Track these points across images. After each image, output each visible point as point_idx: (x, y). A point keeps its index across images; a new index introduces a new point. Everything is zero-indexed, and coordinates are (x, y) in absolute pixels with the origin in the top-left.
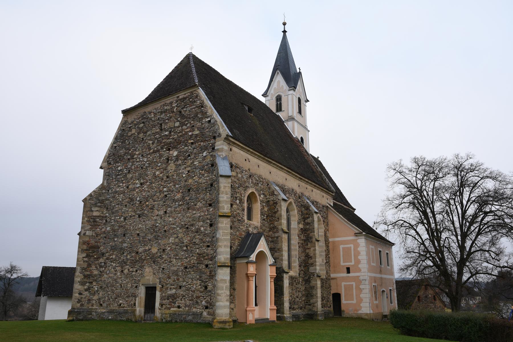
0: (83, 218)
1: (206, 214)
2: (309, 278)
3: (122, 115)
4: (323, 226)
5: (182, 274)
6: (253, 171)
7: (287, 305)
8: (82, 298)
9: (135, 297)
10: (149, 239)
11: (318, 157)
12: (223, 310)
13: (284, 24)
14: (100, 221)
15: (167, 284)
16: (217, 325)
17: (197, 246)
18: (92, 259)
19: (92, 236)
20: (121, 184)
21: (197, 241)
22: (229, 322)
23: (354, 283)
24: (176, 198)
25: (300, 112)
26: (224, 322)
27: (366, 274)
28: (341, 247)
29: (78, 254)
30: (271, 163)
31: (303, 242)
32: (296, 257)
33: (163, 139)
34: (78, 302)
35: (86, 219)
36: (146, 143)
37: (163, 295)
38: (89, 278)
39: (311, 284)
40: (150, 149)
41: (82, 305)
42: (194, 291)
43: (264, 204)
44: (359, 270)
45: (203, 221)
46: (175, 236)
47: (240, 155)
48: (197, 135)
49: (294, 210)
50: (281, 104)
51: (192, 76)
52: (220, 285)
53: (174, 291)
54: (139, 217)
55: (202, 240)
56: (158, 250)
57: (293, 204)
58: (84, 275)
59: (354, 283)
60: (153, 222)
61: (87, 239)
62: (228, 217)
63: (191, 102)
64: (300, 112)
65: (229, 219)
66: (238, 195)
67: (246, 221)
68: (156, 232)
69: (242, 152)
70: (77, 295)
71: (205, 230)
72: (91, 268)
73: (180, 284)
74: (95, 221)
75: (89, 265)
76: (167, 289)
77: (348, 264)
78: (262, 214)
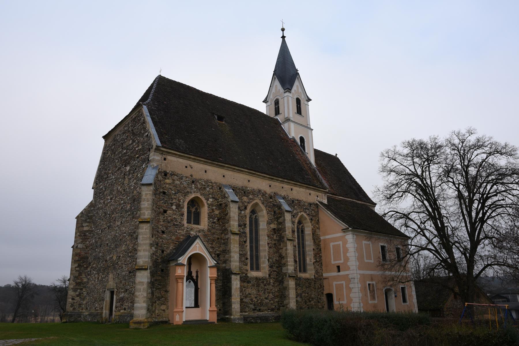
0: (76, 234)
2: (283, 278)
4: (310, 224)
6: (196, 176)
7: (236, 306)
8: (74, 303)
11: (336, 155)
12: (140, 311)
13: (283, 30)
16: (132, 326)
22: (144, 322)
23: (344, 282)
25: (299, 111)
26: (139, 323)
27: (355, 272)
28: (332, 244)
29: (72, 265)
30: (224, 166)
31: (276, 242)
32: (265, 258)
35: (78, 234)
39: (284, 285)
41: (74, 309)
43: (214, 208)
44: (348, 269)
46: (125, 243)
47: (177, 163)
49: (262, 210)
50: (278, 107)
52: (138, 287)
57: (261, 204)
59: (344, 282)
61: (79, 251)
62: (148, 222)
64: (299, 111)
65: (149, 225)
66: (174, 201)
67: (186, 225)
69: (181, 160)
70: (70, 300)
72: (82, 277)
74: (85, 235)
75: (80, 274)
77: (338, 262)
78: (210, 216)
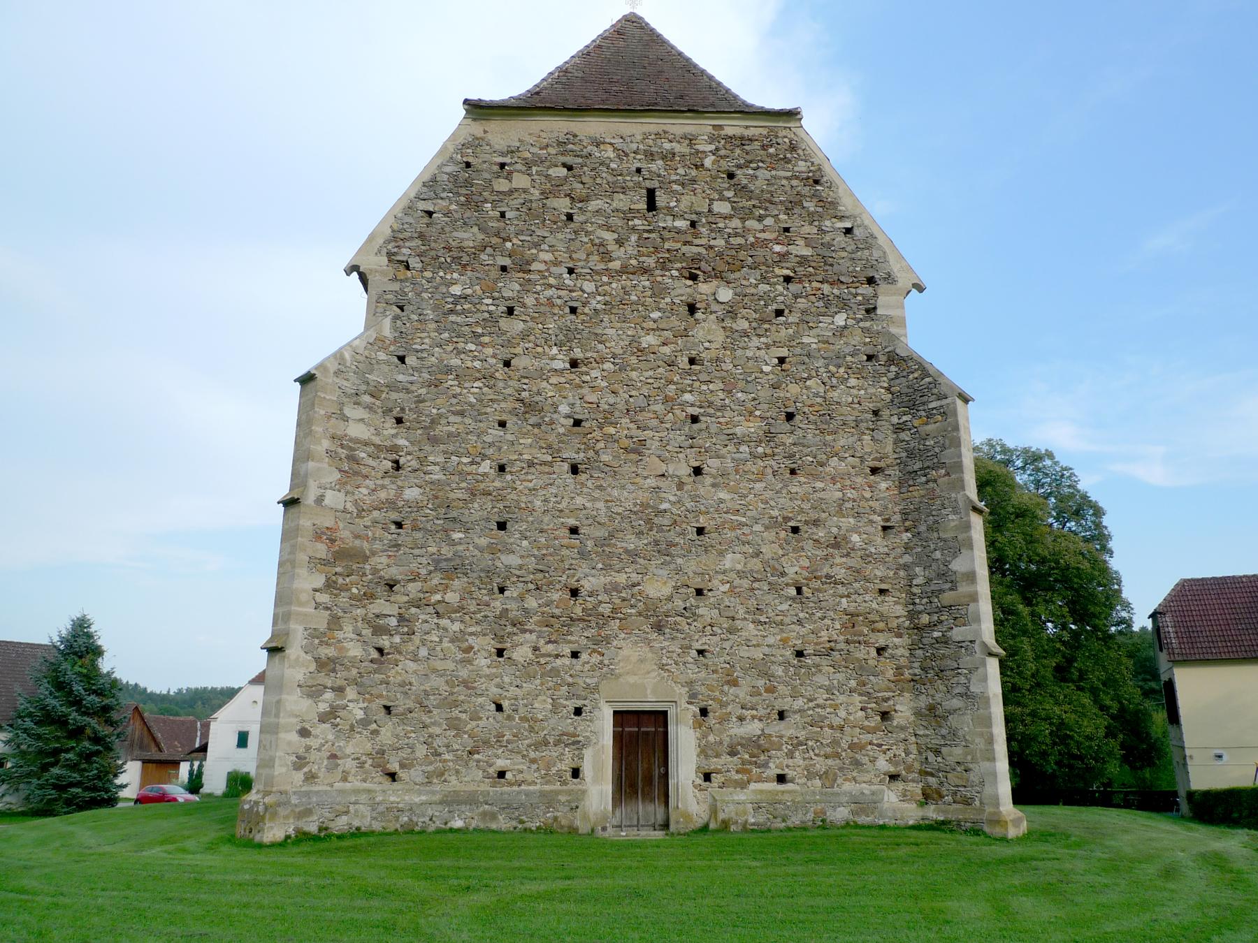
1: (868, 495)
5: (786, 671)
8: (308, 748)
9: (578, 745)
10: (627, 551)
14: (371, 462)
15: (723, 705)
17: (841, 590)
18: (343, 599)
19: (345, 511)
20: (471, 347)
21: (840, 573)
34: (297, 767)
36: (587, 233)
37: (711, 738)
40: (606, 256)
41: (311, 777)
42: (841, 728)
48: (803, 261)
51: (632, 75)
54: (575, 470)
56: (676, 588)
58: (317, 660)
60: (642, 496)
63: (770, 155)
68: (660, 530)
70: (294, 737)
71: (868, 543)
72: (340, 635)
73: (780, 705)
74: (352, 459)
75: (335, 623)
76: (724, 720)
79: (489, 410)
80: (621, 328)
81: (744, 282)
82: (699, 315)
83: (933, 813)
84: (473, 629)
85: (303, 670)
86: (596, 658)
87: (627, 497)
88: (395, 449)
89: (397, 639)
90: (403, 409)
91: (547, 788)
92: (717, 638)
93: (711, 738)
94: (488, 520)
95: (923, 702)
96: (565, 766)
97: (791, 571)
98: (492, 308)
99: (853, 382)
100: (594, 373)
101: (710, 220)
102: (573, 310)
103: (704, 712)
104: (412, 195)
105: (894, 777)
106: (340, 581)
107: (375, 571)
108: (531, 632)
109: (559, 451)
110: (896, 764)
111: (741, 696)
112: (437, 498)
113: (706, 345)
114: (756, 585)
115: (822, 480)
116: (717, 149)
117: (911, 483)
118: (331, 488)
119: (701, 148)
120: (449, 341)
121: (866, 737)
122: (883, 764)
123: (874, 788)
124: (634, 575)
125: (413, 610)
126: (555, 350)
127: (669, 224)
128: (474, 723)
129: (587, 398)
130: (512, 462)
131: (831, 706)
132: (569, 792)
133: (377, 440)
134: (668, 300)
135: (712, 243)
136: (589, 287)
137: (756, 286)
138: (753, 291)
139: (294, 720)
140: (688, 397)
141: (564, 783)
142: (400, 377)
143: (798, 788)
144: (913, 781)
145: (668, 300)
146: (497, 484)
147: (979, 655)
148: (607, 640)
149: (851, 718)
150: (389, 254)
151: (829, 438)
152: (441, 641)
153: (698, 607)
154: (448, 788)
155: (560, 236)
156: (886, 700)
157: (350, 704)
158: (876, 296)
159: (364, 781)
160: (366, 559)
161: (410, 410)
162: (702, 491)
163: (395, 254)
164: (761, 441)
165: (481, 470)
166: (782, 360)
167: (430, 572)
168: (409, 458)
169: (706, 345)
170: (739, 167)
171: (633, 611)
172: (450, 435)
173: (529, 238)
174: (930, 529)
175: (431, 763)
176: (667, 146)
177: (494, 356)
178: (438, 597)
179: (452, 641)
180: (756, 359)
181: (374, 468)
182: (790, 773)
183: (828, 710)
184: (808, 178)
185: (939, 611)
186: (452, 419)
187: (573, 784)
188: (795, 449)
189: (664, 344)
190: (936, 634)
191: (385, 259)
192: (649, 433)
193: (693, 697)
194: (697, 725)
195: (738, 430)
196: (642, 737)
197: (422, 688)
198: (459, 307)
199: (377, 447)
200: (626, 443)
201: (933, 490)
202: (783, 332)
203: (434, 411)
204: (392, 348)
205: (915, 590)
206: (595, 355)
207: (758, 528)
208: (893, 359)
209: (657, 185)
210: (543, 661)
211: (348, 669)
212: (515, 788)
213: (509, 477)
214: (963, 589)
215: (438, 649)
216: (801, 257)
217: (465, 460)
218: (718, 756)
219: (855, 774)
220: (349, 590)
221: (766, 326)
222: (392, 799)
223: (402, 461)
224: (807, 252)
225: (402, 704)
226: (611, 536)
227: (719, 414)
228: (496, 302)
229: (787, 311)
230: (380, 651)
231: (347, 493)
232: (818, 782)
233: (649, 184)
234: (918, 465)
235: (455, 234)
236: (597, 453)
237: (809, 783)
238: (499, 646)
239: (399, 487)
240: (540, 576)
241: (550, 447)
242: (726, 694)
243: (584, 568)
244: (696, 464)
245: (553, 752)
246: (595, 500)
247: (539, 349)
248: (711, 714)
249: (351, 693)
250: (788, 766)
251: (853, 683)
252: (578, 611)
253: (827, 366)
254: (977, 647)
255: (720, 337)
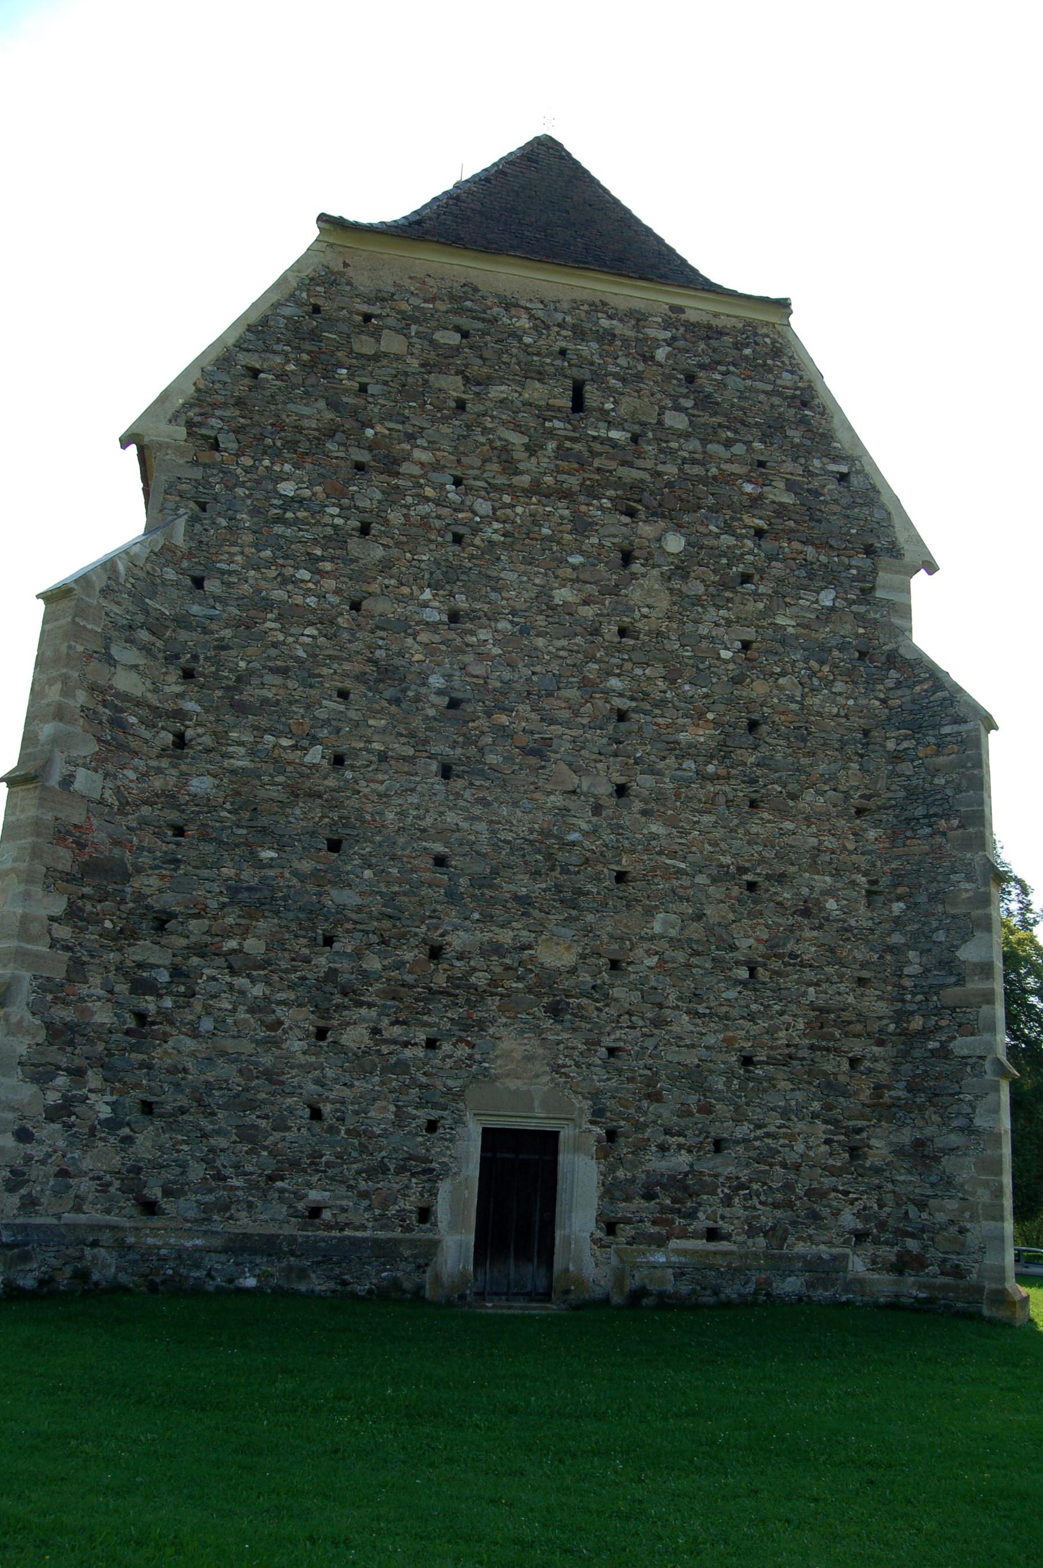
1: (850, 846)
3: (313, 232)
5: (728, 1084)
8: (28, 1159)
9: (431, 1175)
10: (516, 898)
15: (640, 1127)
17: (809, 974)
18: (91, 936)
19: (102, 802)
20: (304, 574)
21: (809, 952)
24: (682, 737)
33: (594, 454)
34: (12, 1187)
36: (485, 431)
37: (620, 1174)
38: (71, 1043)
40: (510, 467)
41: (30, 1203)
42: (797, 1167)
45: (837, 873)
48: (781, 510)
53: (684, 1159)
54: (446, 772)
55: (832, 951)
56: (583, 956)
58: (49, 1025)
68: (565, 871)
71: (847, 911)
72: (83, 990)
73: (715, 1131)
74: (118, 723)
75: (77, 970)
76: (641, 1147)
79: (325, 671)
80: (525, 573)
81: (702, 529)
82: (636, 567)
83: (911, 1287)
84: (281, 996)
85: (28, 1040)
86: (463, 1051)
87: (521, 822)
88: (180, 715)
89: (168, 1003)
90: (195, 657)
91: (381, 1234)
92: (637, 1033)
93: (620, 1174)
94: (313, 834)
95: (906, 1137)
96: (409, 1204)
97: (744, 943)
98: (339, 521)
99: (839, 687)
100: (484, 634)
101: (659, 435)
102: (458, 539)
103: (612, 1135)
104: (231, 342)
105: (860, 1237)
106: (89, 907)
107: (139, 897)
108: (370, 1005)
109: (426, 742)
110: (867, 1219)
111: (666, 1114)
112: (239, 794)
113: (645, 610)
114: (694, 960)
115: (793, 818)
116: (674, 338)
117: (909, 833)
118: (84, 766)
119: (652, 333)
120: (270, 563)
121: (828, 1182)
122: (848, 1219)
123: (835, 1251)
124: (525, 933)
125: (195, 960)
126: (427, 594)
127: (603, 433)
128: (278, 1135)
129: (470, 669)
130: (355, 753)
131: (785, 1136)
132: (413, 1243)
133: (153, 699)
134: (595, 540)
135: (660, 468)
136: (484, 507)
137: (717, 536)
138: (714, 543)
139: (10, 1116)
140: (614, 682)
141: (408, 1229)
142: (195, 609)
143: (734, 1248)
144: (886, 1243)
145: (595, 540)
146: (331, 782)
147: (989, 1076)
148: (481, 1025)
149: (812, 1154)
150: (190, 424)
151: (804, 761)
152: (234, 1010)
153: (612, 986)
154: (232, 1228)
155: (445, 429)
156: (859, 1131)
157: (92, 1096)
158: (874, 571)
159: (108, 1211)
160: (127, 877)
161: (206, 658)
162: (626, 820)
163: (200, 425)
164: (712, 757)
165: (308, 759)
166: (746, 645)
167: (224, 905)
168: (200, 730)
169: (645, 610)
170: (702, 367)
171: (520, 985)
172: (265, 701)
173: (400, 427)
174: (932, 898)
175: (211, 1191)
176: (605, 323)
177: (337, 592)
178: (233, 944)
179: (251, 1011)
180: (713, 639)
181: (146, 741)
182: (726, 1227)
183: (782, 1141)
184: (794, 397)
185: (938, 1011)
186: (269, 678)
187: (420, 1233)
188: (759, 772)
189: (586, 603)
190: (932, 1045)
191: (183, 430)
192: (557, 729)
193: (598, 1113)
194: (603, 1154)
195: (682, 737)
196: (519, 1173)
197: (203, 1078)
198: (289, 515)
199: (154, 709)
200: (524, 740)
201: (940, 847)
202: (751, 606)
203: (242, 664)
204: (185, 564)
205: (907, 983)
206: (486, 607)
207: (701, 879)
208: (893, 660)
209: (588, 376)
210: (385, 1049)
211: (91, 1042)
212: (335, 1233)
213: (349, 775)
214: (975, 985)
215: (230, 1021)
216: (781, 504)
217: (285, 742)
218: (628, 1199)
219: (811, 1231)
220: (102, 922)
221: (728, 594)
222: (150, 1241)
223: (189, 733)
224: (788, 499)
225: (171, 1100)
226: (495, 872)
227: (657, 711)
228: (345, 513)
229: (757, 577)
230: (141, 1017)
231: (106, 775)
232: (761, 1241)
233: (575, 372)
234: (920, 811)
235: (291, 406)
236: (481, 750)
237: (750, 1242)
238: (322, 1023)
239: (183, 774)
240: (387, 924)
241: (412, 735)
242: (645, 1113)
243: (453, 916)
244: (622, 780)
245: (394, 1183)
246: (473, 819)
247: (405, 590)
248: (622, 1140)
249: (94, 1079)
250: (723, 1217)
251: (816, 1106)
252: (440, 980)
253: (806, 660)
254: (988, 1066)
255: (663, 602)
